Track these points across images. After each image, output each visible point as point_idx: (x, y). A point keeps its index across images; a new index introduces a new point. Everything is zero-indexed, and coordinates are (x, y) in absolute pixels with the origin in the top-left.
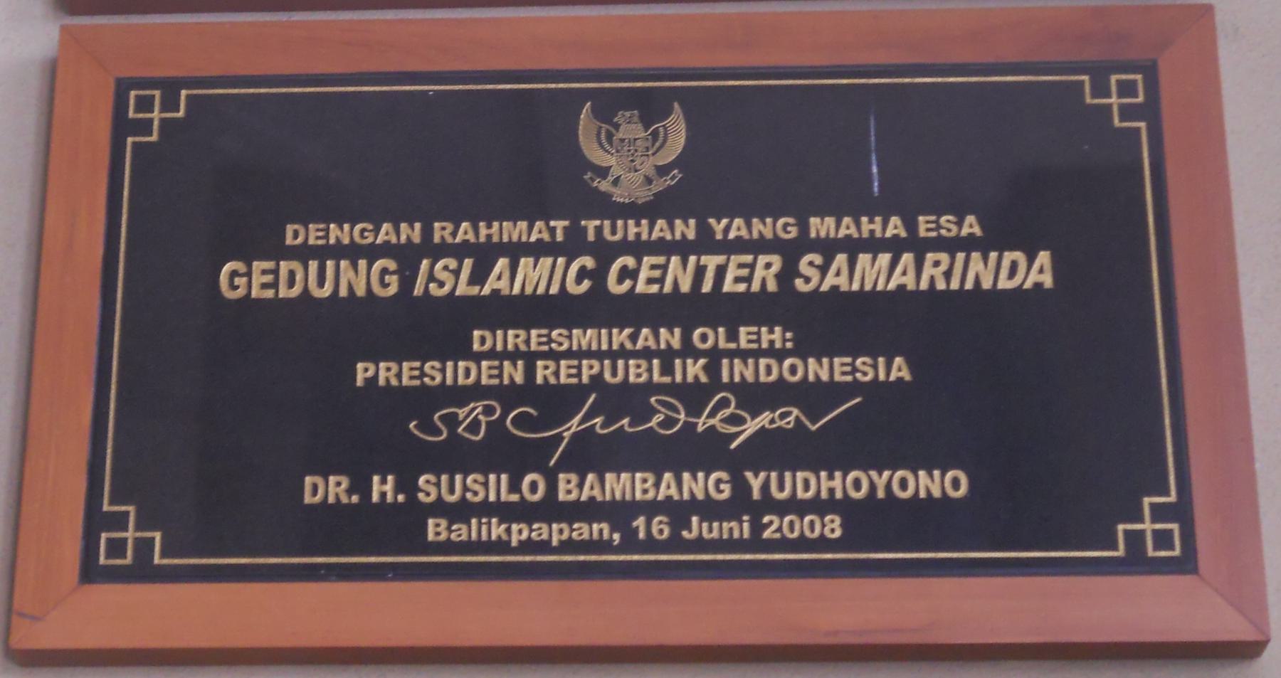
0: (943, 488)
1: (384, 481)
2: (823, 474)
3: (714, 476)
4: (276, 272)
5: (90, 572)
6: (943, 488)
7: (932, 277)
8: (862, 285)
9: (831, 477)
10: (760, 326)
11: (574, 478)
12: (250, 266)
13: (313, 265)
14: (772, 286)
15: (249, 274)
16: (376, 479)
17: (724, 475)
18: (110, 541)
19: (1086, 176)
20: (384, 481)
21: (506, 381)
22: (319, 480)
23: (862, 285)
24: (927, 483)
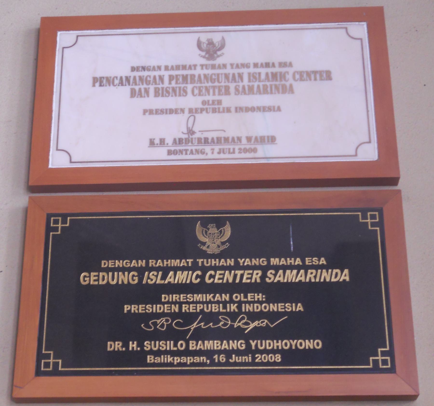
2: (275, 341)
3: (240, 342)
11: (195, 342)
16: (131, 343)
17: (243, 341)
20: (133, 343)
22: (112, 343)
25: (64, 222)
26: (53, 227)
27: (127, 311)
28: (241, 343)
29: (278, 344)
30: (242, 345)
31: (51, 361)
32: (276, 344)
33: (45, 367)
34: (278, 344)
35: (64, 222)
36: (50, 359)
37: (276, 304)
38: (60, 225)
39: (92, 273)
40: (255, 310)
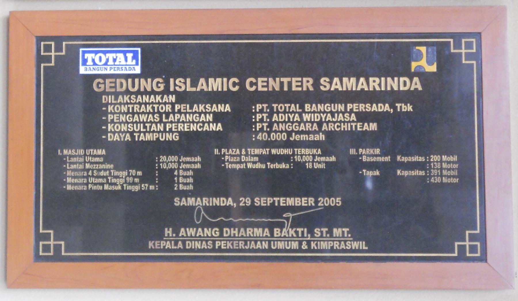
0: (152, 87)
1: (168, 230)
2: (232, 229)
3: (214, 230)
4: (115, 83)
5: (483, 258)
6: (152, 87)
7: (374, 86)
8: (347, 88)
9: (234, 230)
10: (268, 77)
11: (279, 230)
12: (105, 81)
13: (130, 80)
14: (311, 89)
15: (105, 83)
16: (166, 229)
17: (217, 229)
18: (470, 252)
19: (440, 111)
20: (168, 230)
21: (191, 130)
22: (228, 229)
23: (347, 88)
24: (406, 173)
25: (58, 49)
26: (43, 56)
27: (259, 110)
28: (216, 231)
29: (235, 232)
30: (217, 233)
31: (52, 243)
32: (232, 232)
33: (44, 251)
34: (235, 232)
35: (58, 49)
36: (466, 53)
37: (214, 205)
38: (53, 54)
39: (107, 80)
40: (222, 205)
